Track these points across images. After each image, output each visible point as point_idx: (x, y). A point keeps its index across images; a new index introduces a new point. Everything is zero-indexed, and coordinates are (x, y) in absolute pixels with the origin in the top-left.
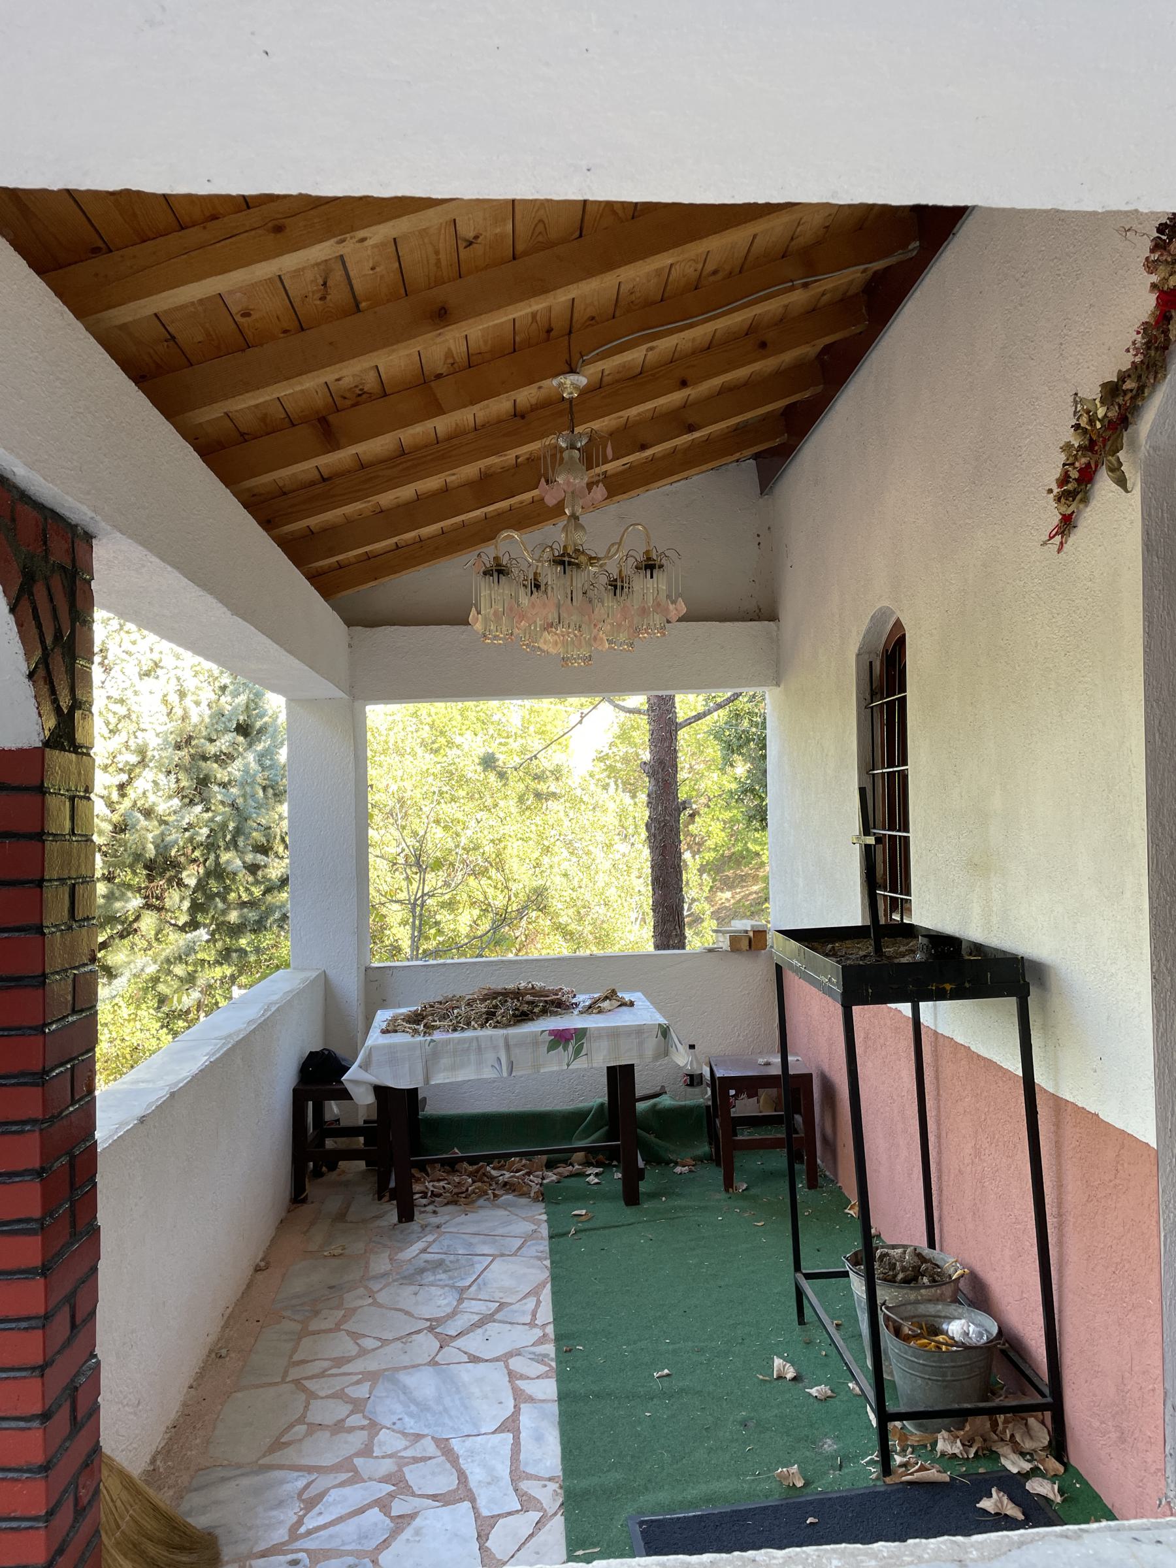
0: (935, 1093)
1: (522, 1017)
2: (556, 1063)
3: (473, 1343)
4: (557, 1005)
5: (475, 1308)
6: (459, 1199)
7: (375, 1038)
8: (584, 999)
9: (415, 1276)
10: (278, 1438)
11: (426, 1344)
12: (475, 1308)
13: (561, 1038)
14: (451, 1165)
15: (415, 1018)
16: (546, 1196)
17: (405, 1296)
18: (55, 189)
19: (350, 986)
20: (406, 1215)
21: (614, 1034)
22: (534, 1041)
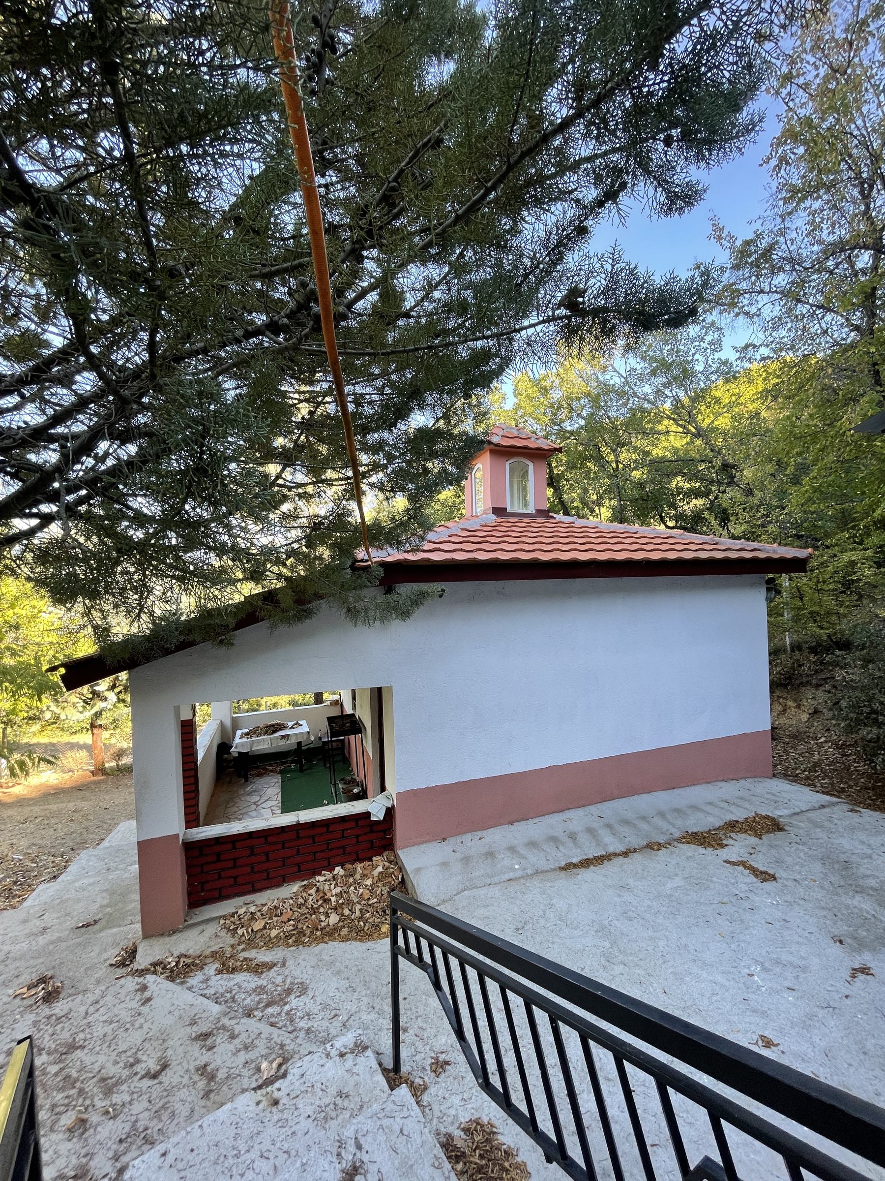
0: (522, 881)
1: (274, 732)
2: (283, 743)
3: (264, 805)
4: (282, 727)
5: (264, 799)
6: (260, 775)
7: (237, 740)
8: (290, 724)
9: (250, 794)
10: (385, 1071)
11: (254, 807)
12: (264, 799)
13: (283, 737)
14: (257, 768)
15: (247, 734)
16: (281, 772)
17: (248, 798)
18: (739, 1175)
19: (228, 723)
20: (246, 781)
21: (296, 735)
22: (277, 738)
